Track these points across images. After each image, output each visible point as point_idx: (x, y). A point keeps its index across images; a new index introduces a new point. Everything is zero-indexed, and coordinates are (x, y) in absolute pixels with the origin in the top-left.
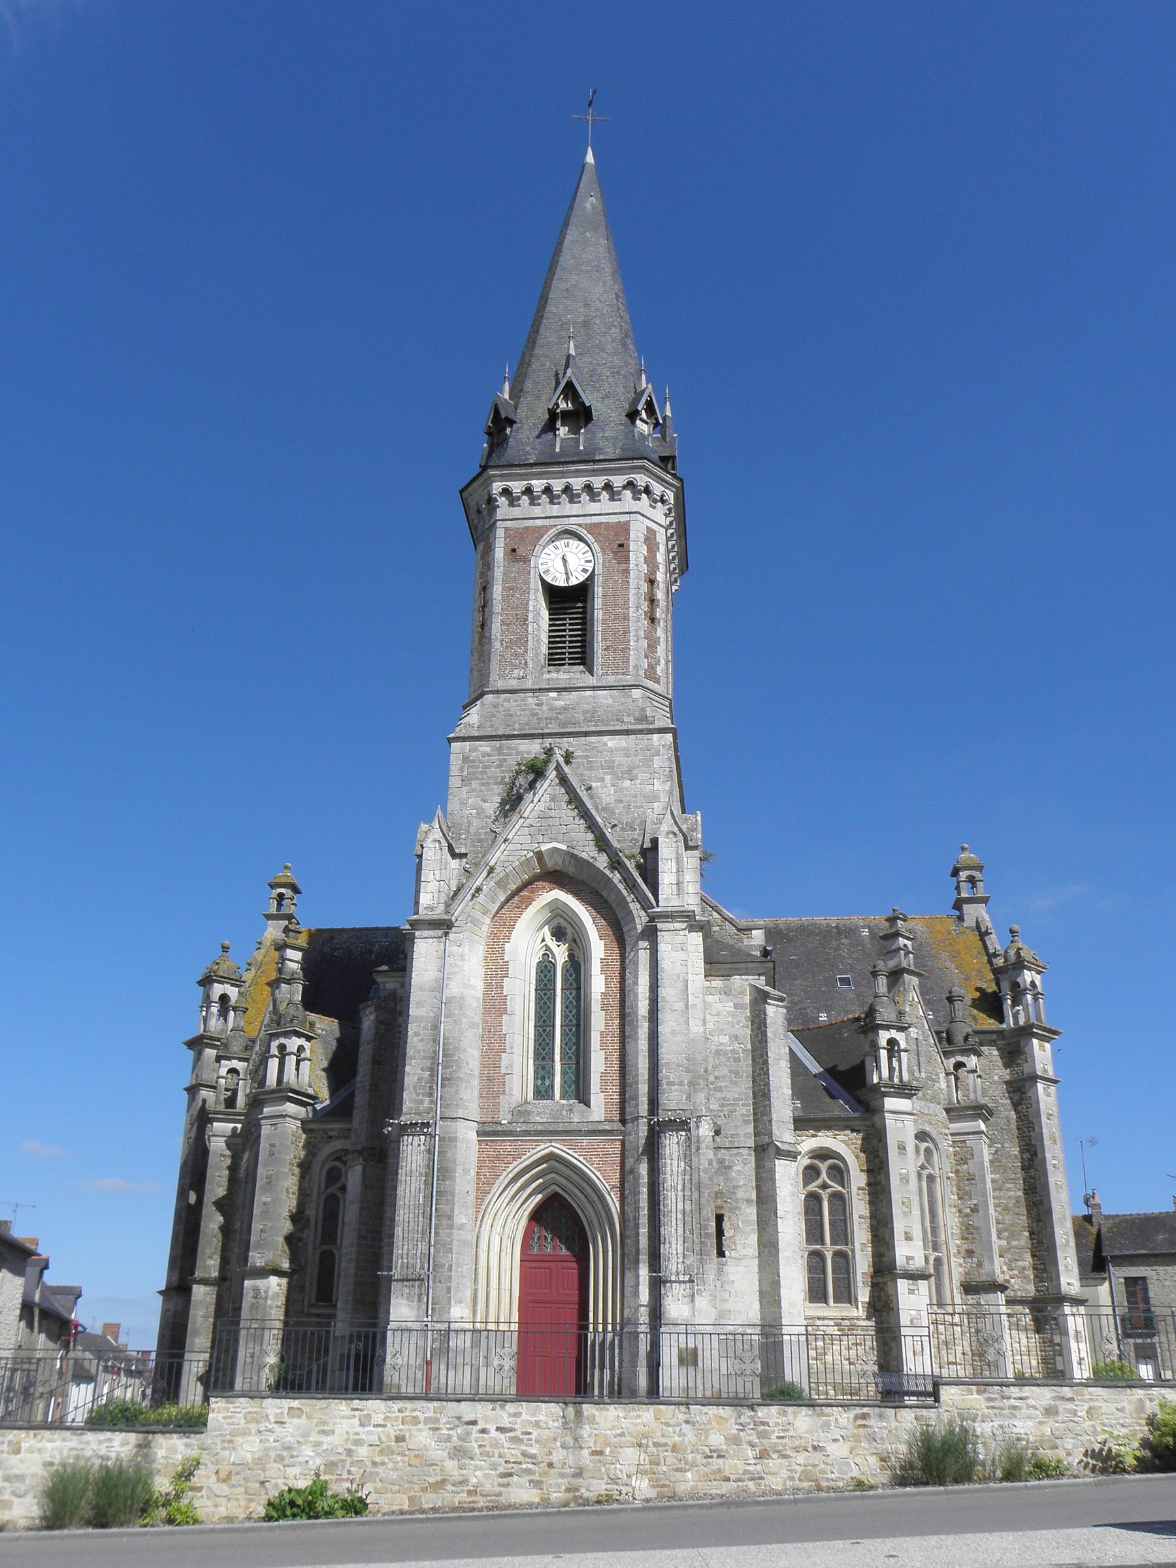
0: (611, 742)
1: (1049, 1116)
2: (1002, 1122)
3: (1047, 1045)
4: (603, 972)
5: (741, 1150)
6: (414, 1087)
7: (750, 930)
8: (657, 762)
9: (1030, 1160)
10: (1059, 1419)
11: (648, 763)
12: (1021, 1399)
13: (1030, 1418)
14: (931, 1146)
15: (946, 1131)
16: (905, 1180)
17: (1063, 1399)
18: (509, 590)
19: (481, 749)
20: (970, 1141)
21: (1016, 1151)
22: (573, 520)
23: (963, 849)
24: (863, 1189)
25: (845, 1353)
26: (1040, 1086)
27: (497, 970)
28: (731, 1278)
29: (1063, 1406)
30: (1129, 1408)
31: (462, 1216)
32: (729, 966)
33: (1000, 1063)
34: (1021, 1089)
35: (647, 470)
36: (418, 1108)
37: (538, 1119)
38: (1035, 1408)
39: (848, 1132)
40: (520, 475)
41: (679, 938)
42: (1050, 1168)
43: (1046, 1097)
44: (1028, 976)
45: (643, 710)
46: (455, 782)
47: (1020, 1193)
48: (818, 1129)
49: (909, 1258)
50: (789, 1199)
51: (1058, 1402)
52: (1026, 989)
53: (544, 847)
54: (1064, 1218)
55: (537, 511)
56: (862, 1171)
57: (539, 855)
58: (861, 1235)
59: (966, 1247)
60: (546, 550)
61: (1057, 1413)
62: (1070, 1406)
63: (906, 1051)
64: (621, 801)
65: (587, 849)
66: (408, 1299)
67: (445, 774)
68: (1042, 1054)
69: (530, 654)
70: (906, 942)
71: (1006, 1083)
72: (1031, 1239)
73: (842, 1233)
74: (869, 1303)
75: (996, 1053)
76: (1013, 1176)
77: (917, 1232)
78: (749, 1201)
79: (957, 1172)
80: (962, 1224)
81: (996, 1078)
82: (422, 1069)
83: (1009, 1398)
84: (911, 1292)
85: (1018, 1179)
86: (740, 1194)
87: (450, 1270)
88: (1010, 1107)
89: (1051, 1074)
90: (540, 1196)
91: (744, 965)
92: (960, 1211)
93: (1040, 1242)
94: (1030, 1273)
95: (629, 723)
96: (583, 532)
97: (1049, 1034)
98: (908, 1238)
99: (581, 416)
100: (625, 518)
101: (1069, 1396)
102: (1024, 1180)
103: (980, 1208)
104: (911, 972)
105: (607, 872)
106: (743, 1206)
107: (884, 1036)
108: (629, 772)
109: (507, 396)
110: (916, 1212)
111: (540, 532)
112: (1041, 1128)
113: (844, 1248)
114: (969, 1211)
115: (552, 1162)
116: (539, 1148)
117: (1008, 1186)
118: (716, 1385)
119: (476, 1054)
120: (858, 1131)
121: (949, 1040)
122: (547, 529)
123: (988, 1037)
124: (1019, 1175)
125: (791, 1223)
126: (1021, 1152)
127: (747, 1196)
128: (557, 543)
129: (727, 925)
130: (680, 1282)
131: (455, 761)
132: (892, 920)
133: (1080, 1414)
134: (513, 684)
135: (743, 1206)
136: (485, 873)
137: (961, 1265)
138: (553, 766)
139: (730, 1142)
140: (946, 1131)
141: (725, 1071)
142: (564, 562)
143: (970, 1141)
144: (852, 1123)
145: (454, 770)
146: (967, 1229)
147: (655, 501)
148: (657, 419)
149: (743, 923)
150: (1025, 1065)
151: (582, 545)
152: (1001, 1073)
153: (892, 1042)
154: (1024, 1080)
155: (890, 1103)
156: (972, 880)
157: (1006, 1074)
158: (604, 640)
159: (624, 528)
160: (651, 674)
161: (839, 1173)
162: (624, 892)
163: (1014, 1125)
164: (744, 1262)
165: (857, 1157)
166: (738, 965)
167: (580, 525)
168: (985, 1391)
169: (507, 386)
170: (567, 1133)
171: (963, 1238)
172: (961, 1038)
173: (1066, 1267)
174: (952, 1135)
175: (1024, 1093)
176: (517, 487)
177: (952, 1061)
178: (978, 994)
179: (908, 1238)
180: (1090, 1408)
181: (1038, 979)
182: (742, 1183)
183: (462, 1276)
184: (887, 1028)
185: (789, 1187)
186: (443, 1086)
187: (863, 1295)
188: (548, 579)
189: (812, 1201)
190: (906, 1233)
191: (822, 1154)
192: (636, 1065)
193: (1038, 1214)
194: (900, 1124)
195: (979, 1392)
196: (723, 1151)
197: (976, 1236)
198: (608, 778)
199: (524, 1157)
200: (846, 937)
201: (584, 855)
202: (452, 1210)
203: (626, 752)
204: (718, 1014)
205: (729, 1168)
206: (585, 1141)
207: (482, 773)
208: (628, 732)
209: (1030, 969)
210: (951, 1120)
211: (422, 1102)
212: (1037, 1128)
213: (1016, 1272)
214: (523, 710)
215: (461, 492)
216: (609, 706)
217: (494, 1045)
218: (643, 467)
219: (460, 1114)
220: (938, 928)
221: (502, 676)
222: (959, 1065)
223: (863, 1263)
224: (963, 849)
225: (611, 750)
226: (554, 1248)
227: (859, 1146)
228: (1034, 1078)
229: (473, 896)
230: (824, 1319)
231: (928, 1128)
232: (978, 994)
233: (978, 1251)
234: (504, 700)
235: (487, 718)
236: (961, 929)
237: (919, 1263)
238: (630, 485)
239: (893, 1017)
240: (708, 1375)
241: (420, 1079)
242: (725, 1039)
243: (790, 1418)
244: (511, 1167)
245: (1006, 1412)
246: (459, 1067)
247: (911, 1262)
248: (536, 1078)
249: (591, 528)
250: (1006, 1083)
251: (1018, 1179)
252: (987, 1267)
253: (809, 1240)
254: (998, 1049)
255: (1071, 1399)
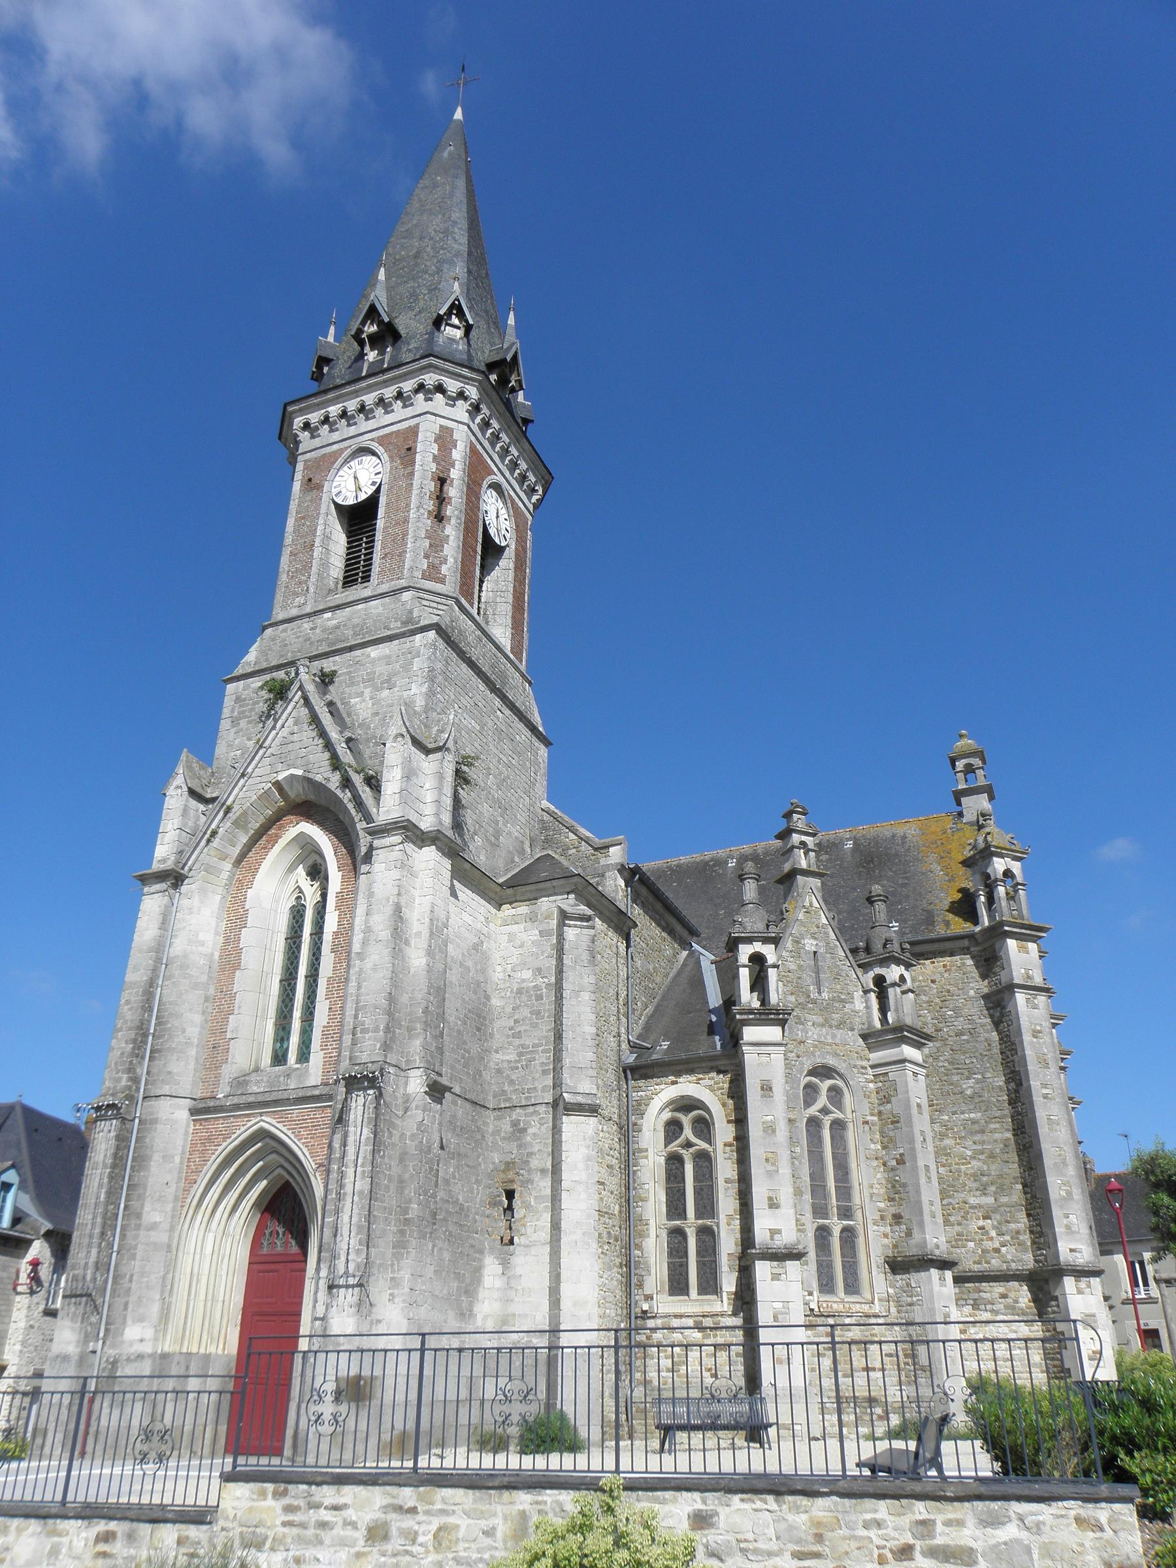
0: (374, 652)
1: (1036, 1034)
2: (982, 1047)
3: (1032, 947)
4: (337, 908)
5: (538, 1108)
6: (116, 1063)
7: (608, 847)
8: (417, 664)
9: (1017, 1091)
10: (389, 1547)
11: (407, 667)
12: (336, 1508)
13: (343, 1543)
14: (840, 1083)
15: (865, 1063)
16: (770, 1129)
17: (399, 1509)
18: (300, 519)
19: (253, 686)
20: (893, 1073)
21: (1000, 1081)
22: (361, 438)
23: (961, 736)
24: (730, 1145)
25: (709, 1362)
26: (1020, 997)
27: (236, 918)
28: (519, 1271)
29: (399, 1523)
30: (502, 1529)
31: (153, 1213)
32: (533, 887)
33: (976, 974)
34: (998, 1003)
35: (437, 367)
36: (115, 1087)
37: (255, 1089)
38: (354, 1525)
39: (714, 1074)
40: (318, 405)
41: (396, 854)
42: (1038, 1100)
43: (1030, 1011)
44: (999, 865)
45: (411, 612)
46: (225, 724)
47: (1009, 1135)
48: (679, 1074)
49: (774, 1232)
50: (581, 1166)
51: (392, 1516)
52: (996, 880)
53: (281, 777)
54: (1064, 1163)
55: (336, 436)
56: (729, 1122)
57: (277, 785)
58: (727, 1203)
59: (893, 1210)
60: (341, 473)
61: (386, 1538)
62: (409, 1522)
63: (775, 966)
64: (377, 714)
65: (322, 770)
66: (72, 1320)
67: (218, 719)
68: (1022, 959)
69: (313, 579)
70: (804, 838)
71: (985, 997)
72: (1025, 1193)
73: (707, 1206)
74: (736, 1293)
75: (970, 962)
76: (998, 1114)
77: (786, 1194)
78: (543, 1171)
79: (880, 1113)
80: (888, 1180)
81: (972, 993)
82: (126, 1043)
83: (317, 1506)
84: (776, 1277)
85: (1004, 1116)
86: (535, 1163)
87: (131, 1281)
88: (990, 1026)
89: (1038, 980)
90: (265, 1182)
91: (548, 884)
92: (884, 1164)
93: (1034, 1197)
94: (1026, 1238)
95: (396, 627)
96: (375, 446)
97: (1030, 932)
98: (773, 1204)
99: (388, 334)
100: (412, 422)
101: (410, 1504)
102: (1012, 1117)
103: (906, 1158)
104: (806, 873)
105: (339, 792)
106: (537, 1177)
107: (745, 952)
108: (388, 681)
109: (331, 339)
110: (785, 1170)
111: (335, 456)
112: (1023, 1050)
113: (708, 1222)
114: (894, 1163)
115: (268, 1140)
116: (250, 1124)
117: (992, 1126)
118: (399, 1426)
119: (198, 1018)
120: (724, 1072)
121: (868, 950)
122: (342, 451)
123: (959, 944)
124: (1007, 1112)
125: (583, 1196)
126: (1007, 1082)
127: (541, 1166)
128: (352, 463)
129: (584, 846)
130: (347, 1287)
131: (228, 702)
132: (788, 815)
133: (421, 1539)
134: (294, 612)
135: (537, 1177)
136: (221, 814)
137: (886, 1236)
138: (295, 688)
139: (526, 1098)
140: (865, 1063)
141: (526, 1012)
142: (352, 482)
143: (893, 1073)
144: (718, 1063)
145: (226, 712)
146: (894, 1187)
147: (454, 399)
148: (467, 321)
149: (598, 842)
150: (1002, 973)
151: (374, 458)
152: (978, 986)
153: (758, 960)
154: (1000, 991)
155: (750, 1033)
156: (969, 770)
157: (984, 987)
158: (383, 548)
159: (414, 431)
160: (433, 573)
161: (704, 1127)
162: (353, 812)
163: (996, 1049)
164: (533, 1251)
165: (724, 1105)
166: (542, 885)
167: (372, 440)
168: (285, 1493)
169: (332, 330)
170: (276, 1102)
171: (891, 1200)
172: (880, 946)
173: (1068, 1227)
174: (872, 1067)
175: (1004, 1008)
176: (314, 417)
177: (871, 974)
178: (960, 895)
179: (773, 1204)
180: (440, 1529)
181: (1016, 867)
182: (536, 1149)
183: (148, 1287)
184: (749, 940)
185: (584, 1150)
186: (151, 1059)
187: (729, 1282)
188: (339, 501)
189: (674, 1162)
190: (770, 1199)
191: (686, 1105)
192: (601, 1017)
193: (1029, 1162)
194: (764, 1059)
195: (277, 1495)
196: (518, 1110)
197: (903, 1196)
198: (367, 691)
199: (234, 1136)
200: (826, 853)
201: (319, 778)
202: (142, 1207)
203: (388, 660)
204: (521, 946)
205: (524, 1130)
206: (296, 1111)
207: (251, 710)
208: (390, 638)
209: (1002, 856)
210: (871, 1048)
211: (120, 1079)
212: (1019, 1050)
213: (1008, 1238)
214: (298, 637)
215: (280, 438)
216: (379, 615)
217: (222, 1005)
218: (430, 366)
219: (166, 1090)
220: (933, 828)
221: (284, 607)
222: (880, 981)
223: (728, 1243)
224: (961, 736)
225: (373, 662)
226: (286, 1244)
227: (726, 1091)
228: (1011, 987)
229: (209, 841)
230: (681, 1316)
231: (831, 1061)
232: (960, 895)
233: (906, 1215)
234: (283, 631)
235: (263, 652)
236: (959, 826)
237: (788, 1237)
238: (421, 387)
239: (760, 926)
240: (388, 1411)
241: (123, 1053)
242: (527, 974)
243: (11, 1538)
244: (220, 1149)
245: (311, 1532)
246: (171, 1036)
247: (777, 1237)
248: (275, 1041)
249: (381, 441)
250: (985, 997)
251: (1004, 1116)
252: (917, 1235)
253: (670, 1216)
254: (973, 958)
255: (413, 1510)
